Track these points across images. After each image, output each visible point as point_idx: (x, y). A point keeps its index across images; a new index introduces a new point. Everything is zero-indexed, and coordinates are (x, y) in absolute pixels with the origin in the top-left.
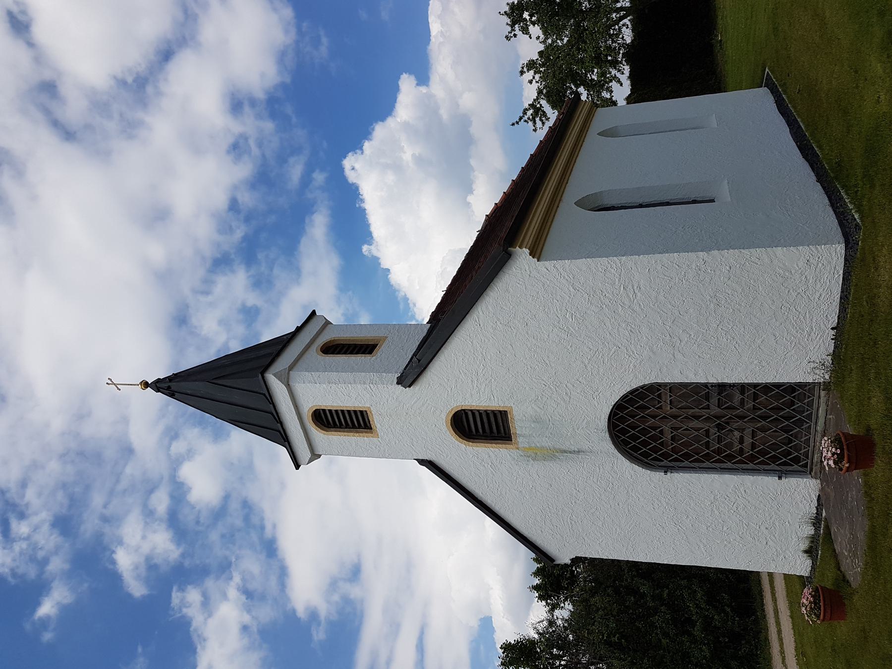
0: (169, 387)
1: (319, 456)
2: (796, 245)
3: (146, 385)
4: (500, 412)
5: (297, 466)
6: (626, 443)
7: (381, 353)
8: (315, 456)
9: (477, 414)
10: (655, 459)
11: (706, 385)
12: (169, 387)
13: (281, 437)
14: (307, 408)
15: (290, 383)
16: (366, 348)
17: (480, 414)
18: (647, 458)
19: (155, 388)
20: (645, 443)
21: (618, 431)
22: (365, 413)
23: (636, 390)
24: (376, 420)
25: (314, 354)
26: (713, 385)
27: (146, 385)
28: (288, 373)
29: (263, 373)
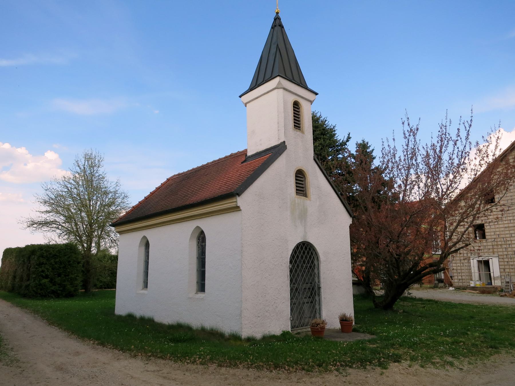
3: (277, 13)
12: (275, 26)
19: (276, 18)
25: (292, 99)
28: (281, 88)
29: (279, 76)
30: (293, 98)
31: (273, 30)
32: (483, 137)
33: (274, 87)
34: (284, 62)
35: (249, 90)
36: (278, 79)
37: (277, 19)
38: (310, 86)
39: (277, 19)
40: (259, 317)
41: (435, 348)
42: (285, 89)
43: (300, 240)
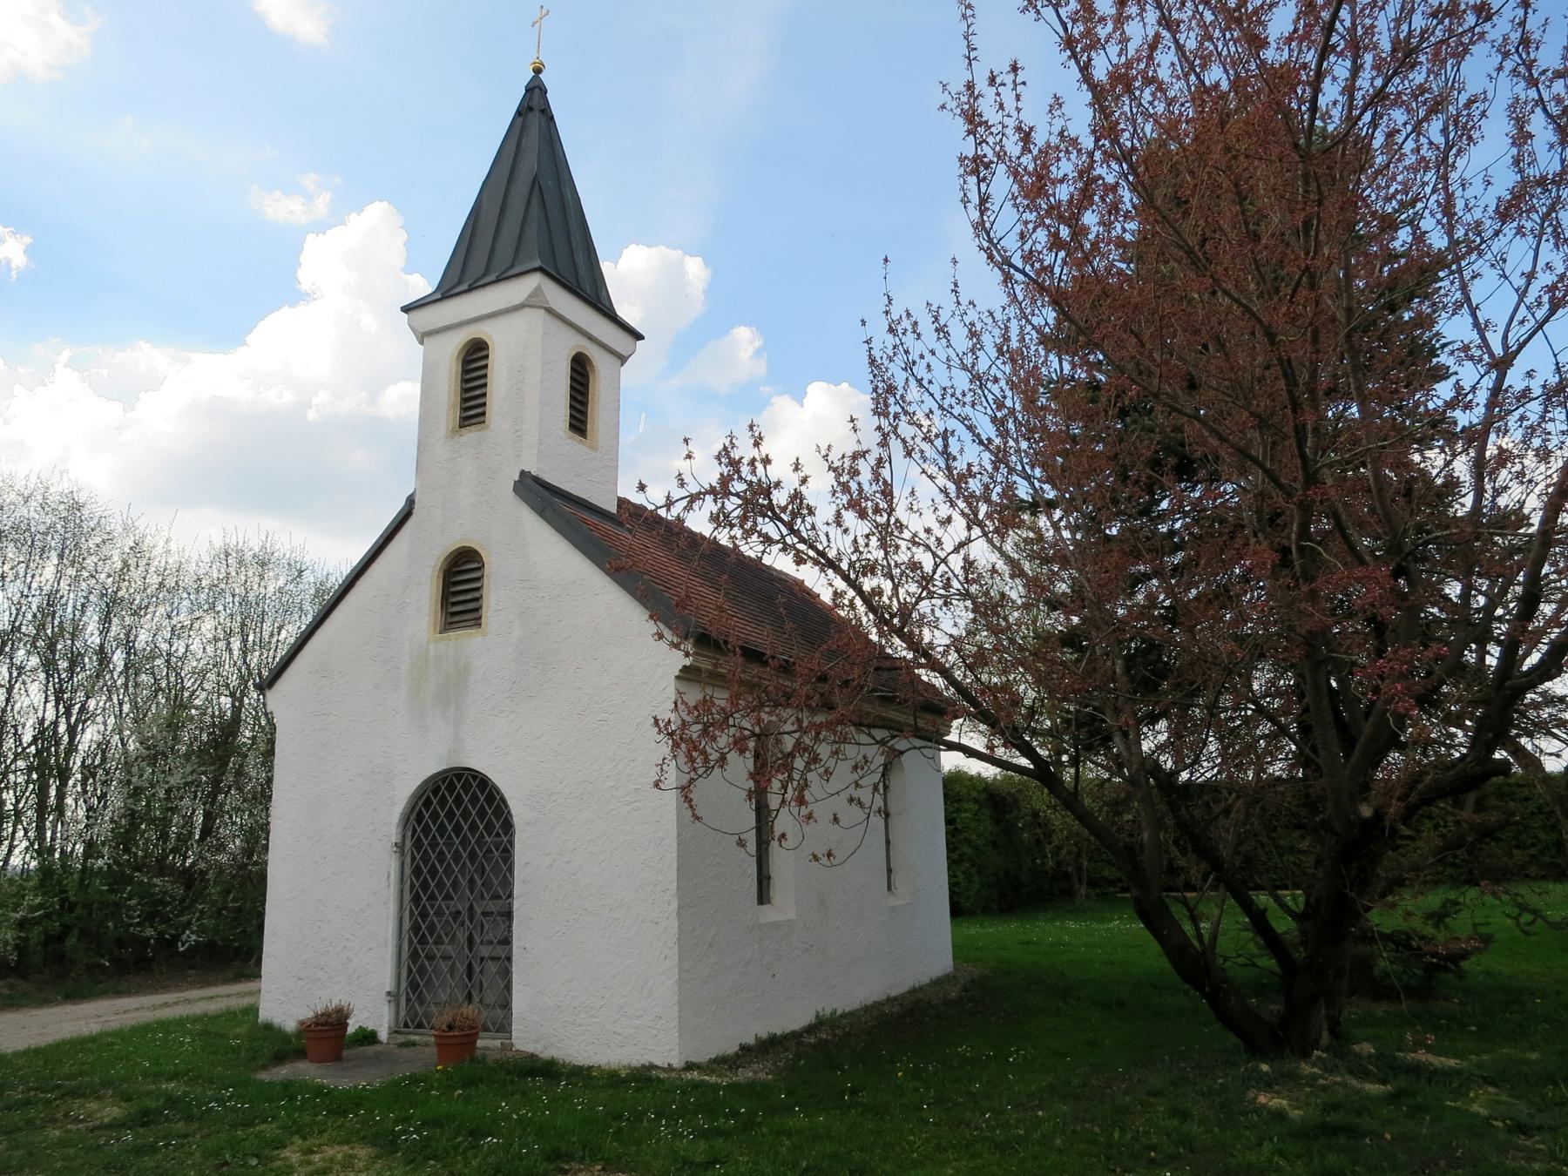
0: (531, 109)
1: (421, 343)
2: (680, 1002)
3: (538, 71)
4: (480, 618)
5: (407, 309)
6: (436, 791)
7: (572, 443)
8: (422, 337)
9: (476, 595)
10: (414, 831)
11: (510, 896)
12: (531, 109)
13: (448, 289)
14: (491, 333)
15: (527, 310)
16: (579, 423)
17: (478, 589)
18: (424, 805)
19: (532, 85)
20: (434, 817)
21: (452, 780)
22: (481, 419)
23: (506, 806)
24: (471, 435)
25: (572, 344)
26: (510, 905)
27: (538, 71)
28: (539, 307)
29: (540, 269)
30: (576, 343)
31: (520, 120)
32: (886, 260)
33: (517, 302)
34: (500, 199)
35: (439, 296)
36: (535, 280)
37: (536, 93)
38: (623, 311)
39: (536, 93)
40: (300, 979)
41: (1334, 39)
42: (549, 311)
43: (433, 767)
